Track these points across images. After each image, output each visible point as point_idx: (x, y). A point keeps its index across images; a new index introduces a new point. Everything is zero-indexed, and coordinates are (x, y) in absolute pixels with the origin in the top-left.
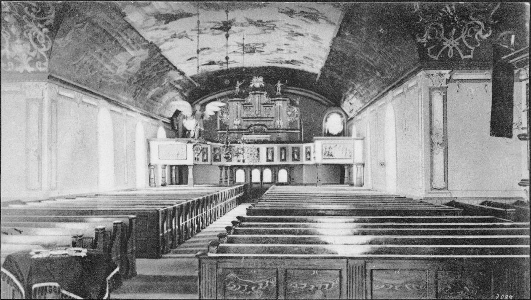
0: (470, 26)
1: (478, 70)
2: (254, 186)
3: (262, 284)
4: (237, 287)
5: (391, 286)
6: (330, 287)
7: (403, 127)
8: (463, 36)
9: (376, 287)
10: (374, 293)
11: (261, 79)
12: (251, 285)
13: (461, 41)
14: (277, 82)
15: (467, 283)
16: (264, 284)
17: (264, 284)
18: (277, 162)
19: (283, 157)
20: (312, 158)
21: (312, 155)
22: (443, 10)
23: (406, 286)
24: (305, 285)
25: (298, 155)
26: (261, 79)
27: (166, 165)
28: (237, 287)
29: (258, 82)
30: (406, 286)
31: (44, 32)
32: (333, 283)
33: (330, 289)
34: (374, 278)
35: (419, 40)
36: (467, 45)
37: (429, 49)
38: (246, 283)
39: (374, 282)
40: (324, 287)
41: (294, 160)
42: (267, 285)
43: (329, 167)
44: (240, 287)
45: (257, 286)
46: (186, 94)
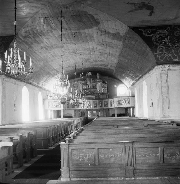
0: (176, 47)
2: (89, 118)
3: (88, 156)
4: (77, 157)
5: (144, 155)
6: (117, 156)
7: (150, 91)
9: (137, 156)
10: (137, 158)
11: (90, 73)
12: (83, 156)
13: (172, 53)
14: (97, 74)
15: (177, 152)
16: (89, 156)
17: (89, 156)
18: (98, 107)
19: (101, 105)
20: (113, 105)
21: (113, 104)
22: (164, 40)
23: (151, 154)
24: (107, 155)
25: (107, 104)
26: (90, 73)
27: (52, 110)
28: (77, 157)
29: (89, 74)
30: (151, 154)
32: (119, 155)
33: (118, 157)
34: (137, 152)
35: (155, 53)
36: (175, 55)
37: (159, 57)
38: (81, 155)
39: (136, 154)
40: (115, 156)
41: (105, 106)
42: (90, 156)
43: (17, 122)
44: (79, 157)
45: (86, 157)
46: (176, 60)
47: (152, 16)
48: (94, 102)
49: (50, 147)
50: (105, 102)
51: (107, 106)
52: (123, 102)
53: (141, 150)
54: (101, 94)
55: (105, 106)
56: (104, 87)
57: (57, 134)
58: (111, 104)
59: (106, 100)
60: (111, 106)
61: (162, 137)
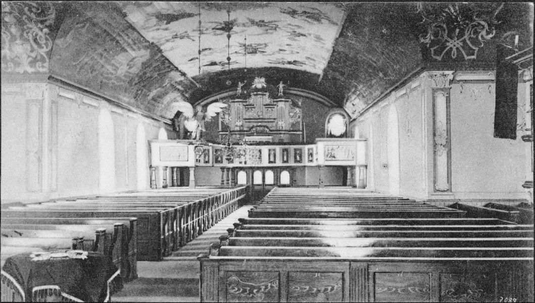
0: (473, 26)
2: (256, 188)
3: (264, 287)
4: (239, 290)
5: (394, 289)
6: (332, 289)
7: (406, 128)
8: (466, 37)
9: (378, 290)
10: (377, 296)
11: (263, 80)
13: (464, 42)
14: (279, 83)
15: (471, 285)
16: (266, 287)
17: (266, 287)
18: (279, 163)
19: (285, 159)
20: (314, 160)
21: (315, 157)
22: (447, 10)
23: (409, 289)
24: (308, 288)
25: (301, 156)
26: (263, 80)
27: (167, 167)
28: (239, 290)
29: (260, 83)
30: (409, 289)
32: (336, 286)
34: (377, 281)
35: (422, 40)
36: (471, 45)
37: (432, 49)
38: (248, 286)
39: (376, 285)
40: (326, 290)
41: (296, 161)
42: (269, 288)
43: (331, 169)
44: (241, 290)
45: (259, 289)
47: (235, 13)
49: (164, 256)
53: (387, 277)
57: (175, 230)
61: (34, 247)
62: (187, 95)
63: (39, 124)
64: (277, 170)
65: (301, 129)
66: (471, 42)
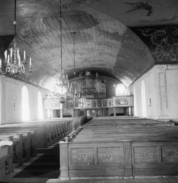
0: (174, 46)
1: (51, 78)
2: (88, 117)
3: (87, 155)
4: (77, 156)
6: (116, 155)
7: (148, 91)
8: (171, 51)
9: (136, 155)
10: (135, 157)
11: (89, 72)
13: (170, 53)
14: (96, 73)
15: (175, 152)
16: (88, 155)
17: (88, 155)
18: (97, 107)
19: (100, 105)
20: (112, 105)
21: (112, 104)
22: (162, 40)
23: (149, 154)
24: (106, 155)
25: (106, 104)
26: (89, 72)
27: (51, 110)
28: (77, 156)
29: (88, 73)
30: (149, 154)
31: (25, 30)
32: (118, 154)
33: (116, 156)
34: (135, 151)
35: (153, 53)
36: (173, 54)
37: (158, 57)
38: (80, 155)
39: (135, 153)
40: (113, 155)
41: (104, 106)
42: (89, 155)
44: (78, 156)
45: (85, 156)
47: (151, 16)
48: (93, 101)
50: (104, 101)
51: (106, 105)
52: (122, 102)
53: (139, 149)
54: (100, 93)
55: (104, 106)
56: (103, 87)
58: (110, 103)
59: (105, 99)
60: (110, 105)
62: (175, 60)
63: (108, 79)
64: (97, 110)
65: (106, 92)
66: (173, 53)
